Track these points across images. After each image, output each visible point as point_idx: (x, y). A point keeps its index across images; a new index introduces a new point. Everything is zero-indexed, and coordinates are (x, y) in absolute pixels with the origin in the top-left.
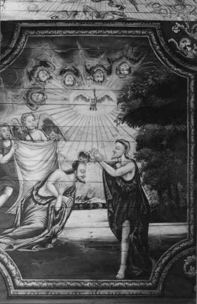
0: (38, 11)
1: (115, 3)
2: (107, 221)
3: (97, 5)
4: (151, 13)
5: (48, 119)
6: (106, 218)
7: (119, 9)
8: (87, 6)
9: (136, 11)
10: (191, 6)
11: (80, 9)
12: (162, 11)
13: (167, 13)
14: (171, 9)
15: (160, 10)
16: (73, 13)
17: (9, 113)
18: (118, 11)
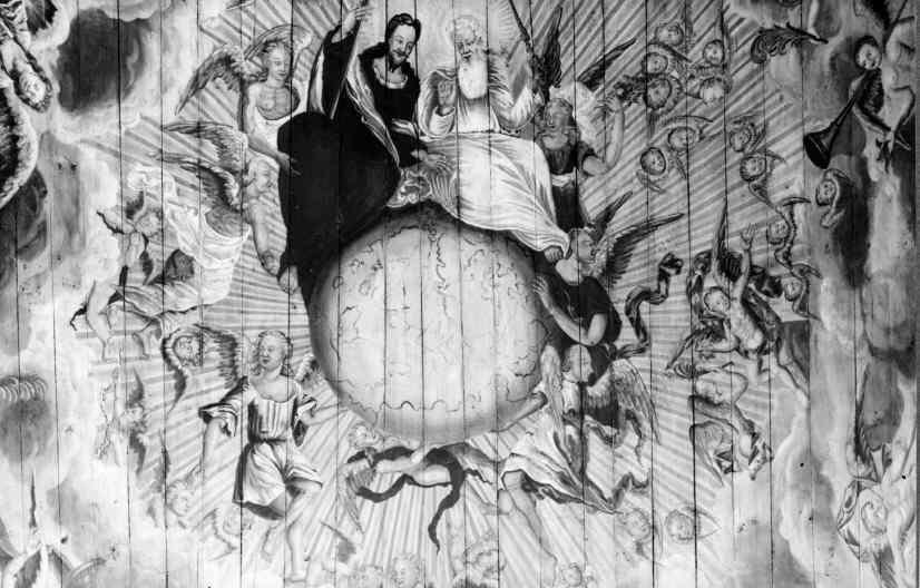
0: (695, 511)
1: (653, 286)
2: (305, 326)
3: (661, 338)
4: (687, 176)
5: (122, 91)
6: (307, 323)
7: (678, 272)
8: (668, 367)
9: (684, 221)
10: (646, 58)
11: (682, 387)
12: (677, 143)
13: (686, 128)
14: (662, 119)
15: (671, 149)
16: (699, 405)
17: (838, 303)
18: (684, 275)
